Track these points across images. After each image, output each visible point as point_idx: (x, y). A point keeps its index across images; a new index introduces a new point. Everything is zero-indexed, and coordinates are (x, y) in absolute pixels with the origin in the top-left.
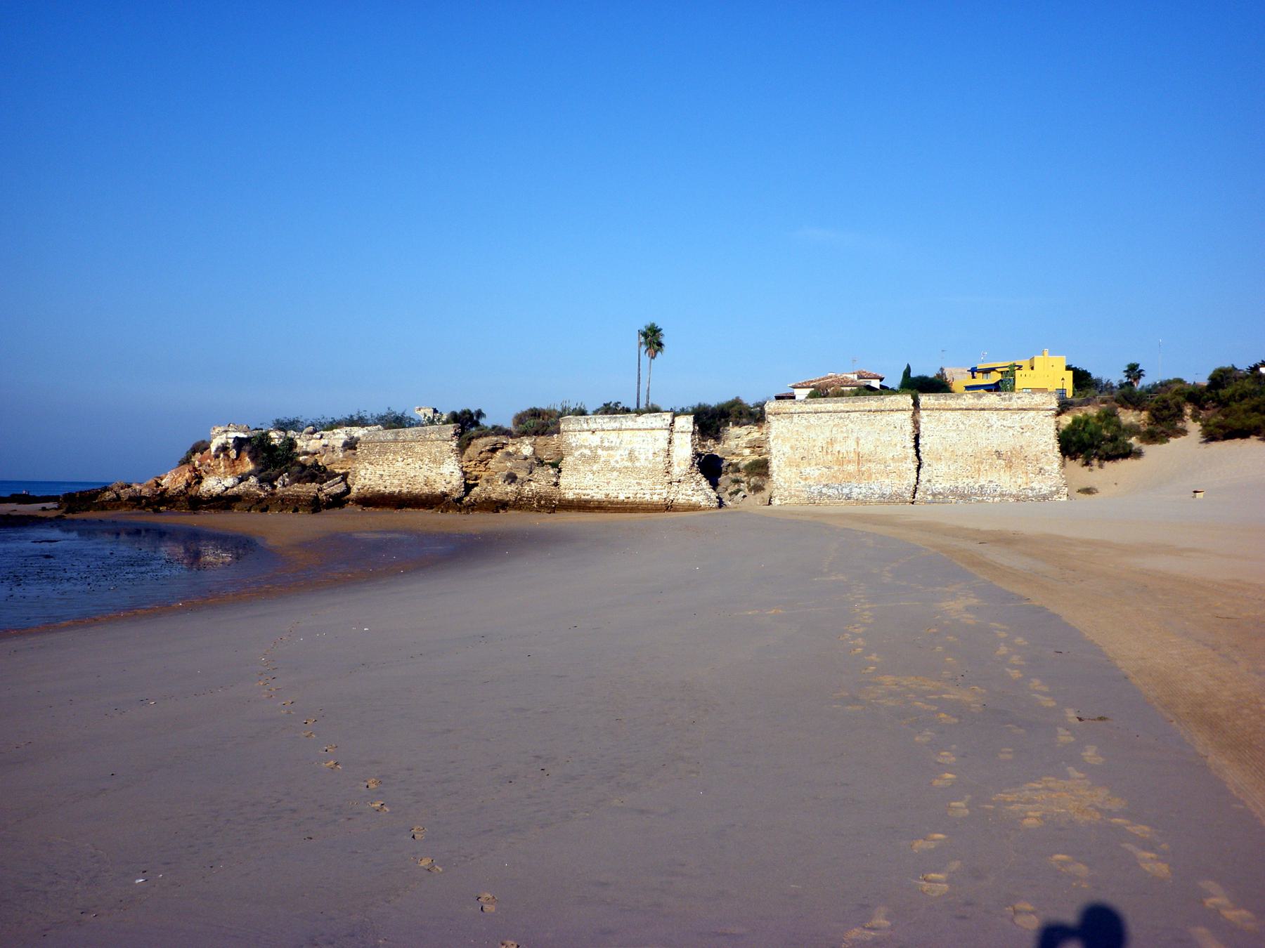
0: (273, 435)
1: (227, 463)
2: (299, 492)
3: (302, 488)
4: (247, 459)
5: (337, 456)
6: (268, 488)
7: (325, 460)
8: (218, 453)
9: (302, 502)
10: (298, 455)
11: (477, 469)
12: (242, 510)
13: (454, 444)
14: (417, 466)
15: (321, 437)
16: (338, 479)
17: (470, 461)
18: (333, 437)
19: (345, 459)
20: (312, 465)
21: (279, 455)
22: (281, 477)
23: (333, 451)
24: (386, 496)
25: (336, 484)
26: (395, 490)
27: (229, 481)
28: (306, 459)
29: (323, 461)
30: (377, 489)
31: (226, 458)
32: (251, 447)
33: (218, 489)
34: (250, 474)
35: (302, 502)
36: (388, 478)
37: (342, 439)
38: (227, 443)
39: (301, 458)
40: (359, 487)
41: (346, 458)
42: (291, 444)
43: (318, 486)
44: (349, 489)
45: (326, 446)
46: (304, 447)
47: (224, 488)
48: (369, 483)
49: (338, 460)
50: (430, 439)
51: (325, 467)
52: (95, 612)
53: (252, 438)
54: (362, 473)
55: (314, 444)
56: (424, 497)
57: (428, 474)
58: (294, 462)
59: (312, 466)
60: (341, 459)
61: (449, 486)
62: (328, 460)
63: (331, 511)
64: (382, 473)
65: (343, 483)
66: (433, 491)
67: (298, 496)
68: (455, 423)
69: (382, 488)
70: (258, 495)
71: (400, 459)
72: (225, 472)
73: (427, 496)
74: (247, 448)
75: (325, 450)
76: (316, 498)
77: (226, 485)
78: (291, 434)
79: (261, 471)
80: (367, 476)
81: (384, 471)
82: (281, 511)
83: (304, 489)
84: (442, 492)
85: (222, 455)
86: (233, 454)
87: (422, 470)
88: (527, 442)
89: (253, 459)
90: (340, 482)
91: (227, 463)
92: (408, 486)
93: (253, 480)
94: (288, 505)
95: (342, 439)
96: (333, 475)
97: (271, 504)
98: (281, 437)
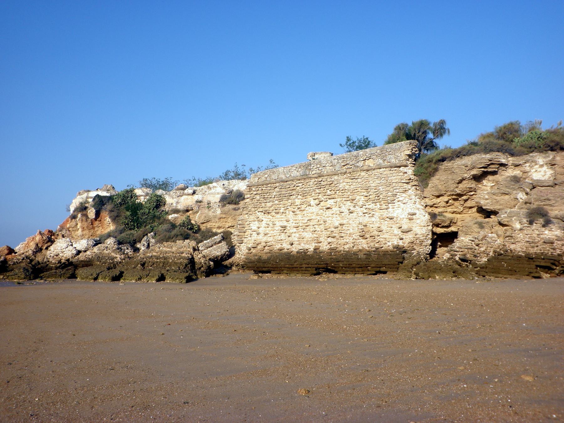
0: (138, 192)
1: (85, 224)
2: (166, 252)
3: (172, 247)
4: (108, 219)
5: (213, 212)
6: (129, 251)
7: (199, 218)
8: (76, 213)
9: (170, 266)
10: (167, 213)
11: (449, 209)
12: (87, 277)
13: (410, 171)
14: (344, 209)
15: (194, 193)
16: (218, 238)
17: (438, 197)
18: (208, 192)
19: (224, 216)
20: (184, 223)
21: (144, 214)
22: (145, 238)
23: (209, 207)
24: (293, 256)
25: (215, 244)
26: (307, 247)
27: (81, 244)
28: (176, 218)
29: (196, 219)
30: (278, 246)
31: (84, 218)
32: (113, 206)
33: (69, 253)
34: (109, 236)
35: (170, 266)
36: (295, 230)
37: (218, 193)
38: (87, 202)
39: (170, 217)
40: (250, 246)
41: (225, 214)
42: (159, 203)
43: (193, 243)
44: (232, 253)
45: (200, 202)
46: (174, 205)
47: (74, 252)
48: (265, 239)
49: (215, 217)
50: (365, 168)
51: (199, 226)
52: (305, 195)
53: (114, 196)
54: (254, 226)
55: (186, 201)
56: (361, 256)
57: (366, 219)
58: (161, 221)
59: (183, 225)
60: (219, 217)
61: (408, 238)
62: (203, 217)
63: (212, 279)
64: (285, 224)
65: (223, 244)
66: (377, 245)
67: (165, 258)
68: (408, 139)
69: (286, 246)
70: (113, 259)
71: (313, 202)
72: (83, 235)
73: (368, 254)
74: (109, 206)
75: (199, 207)
76: (192, 261)
77: (78, 248)
78: (160, 192)
79: (121, 232)
80: (260, 230)
81: (288, 221)
82: (140, 279)
83: (174, 249)
84: (397, 247)
85: (79, 216)
86: (91, 213)
87: (355, 214)
88: (541, 161)
89: (115, 219)
90: (220, 242)
91: (85, 224)
92: (330, 240)
93: (110, 241)
94: (150, 270)
95: (218, 193)
96: (209, 234)
97: (127, 270)
98: (147, 194)
